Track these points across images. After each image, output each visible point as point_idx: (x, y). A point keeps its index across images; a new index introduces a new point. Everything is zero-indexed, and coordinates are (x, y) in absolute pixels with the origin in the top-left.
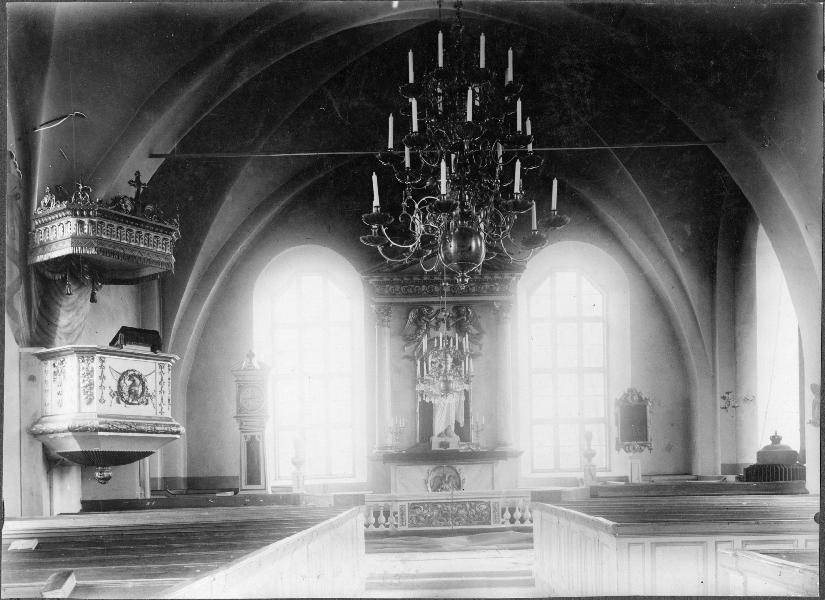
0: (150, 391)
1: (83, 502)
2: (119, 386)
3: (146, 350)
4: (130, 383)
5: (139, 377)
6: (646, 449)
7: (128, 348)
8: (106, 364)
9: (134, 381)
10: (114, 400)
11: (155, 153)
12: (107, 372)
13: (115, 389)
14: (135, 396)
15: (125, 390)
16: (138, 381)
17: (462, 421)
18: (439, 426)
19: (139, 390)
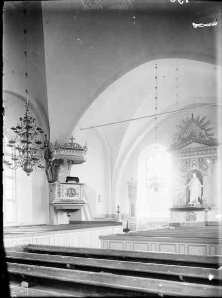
0: (77, 192)
1: (70, 221)
3: (75, 182)
7: (69, 182)
11: (82, 128)
13: (66, 192)
15: (69, 193)
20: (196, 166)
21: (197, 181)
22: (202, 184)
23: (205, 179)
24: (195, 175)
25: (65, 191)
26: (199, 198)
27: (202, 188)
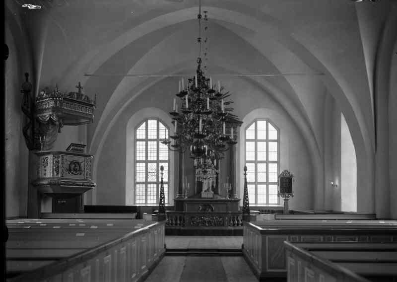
0: (83, 169)
2: (70, 167)
5: (78, 163)
6: (291, 197)
10: (67, 173)
14: (75, 170)
15: (72, 168)
16: (77, 164)
17: (215, 185)
18: (205, 188)
19: (78, 168)
25: (67, 164)
26: (213, 186)
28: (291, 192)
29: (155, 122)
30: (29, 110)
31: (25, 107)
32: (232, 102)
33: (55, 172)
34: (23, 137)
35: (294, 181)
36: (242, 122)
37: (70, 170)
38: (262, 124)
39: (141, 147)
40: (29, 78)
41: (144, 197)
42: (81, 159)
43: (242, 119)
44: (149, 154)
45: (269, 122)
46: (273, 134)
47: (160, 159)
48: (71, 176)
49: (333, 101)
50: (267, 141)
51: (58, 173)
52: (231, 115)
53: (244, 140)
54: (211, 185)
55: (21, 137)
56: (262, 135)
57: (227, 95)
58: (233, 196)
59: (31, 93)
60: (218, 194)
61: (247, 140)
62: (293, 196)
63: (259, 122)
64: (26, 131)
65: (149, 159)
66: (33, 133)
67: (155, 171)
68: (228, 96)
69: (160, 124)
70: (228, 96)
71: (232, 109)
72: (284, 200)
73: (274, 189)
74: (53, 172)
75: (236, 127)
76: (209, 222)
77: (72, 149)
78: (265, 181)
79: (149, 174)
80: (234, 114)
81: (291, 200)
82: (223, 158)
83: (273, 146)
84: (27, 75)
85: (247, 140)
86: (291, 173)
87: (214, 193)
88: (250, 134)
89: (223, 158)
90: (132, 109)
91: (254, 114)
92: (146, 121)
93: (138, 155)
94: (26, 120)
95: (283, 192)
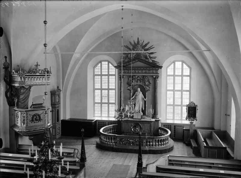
0: (42, 118)
4: (35, 117)
8: (28, 114)
9: (37, 117)
12: (29, 116)
16: (38, 117)
17: (144, 109)
19: (38, 118)
20: (140, 82)
21: (140, 95)
22: (145, 97)
23: (149, 94)
24: (139, 89)
26: (142, 109)
27: (145, 102)
28: (196, 118)
29: (107, 63)
30: (8, 80)
31: (6, 78)
32: (155, 53)
33: (22, 123)
34: (5, 98)
35: (198, 109)
36: (162, 67)
37: (32, 120)
38: (178, 64)
39: (105, 71)
40: (7, 59)
41: (100, 112)
42: (40, 112)
43: (162, 64)
44: (103, 84)
45: (183, 63)
46: (187, 71)
47: (110, 87)
48: (33, 124)
49: (227, 85)
50: (182, 76)
51: (24, 124)
52: (154, 61)
53: (165, 75)
54: (141, 109)
55: (4, 96)
56: (105, 72)
57: (152, 47)
58: (156, 117)
59: (9, 69)
60: (145, 114)
61: (167, 76)
62: (196, 120)
63: (176, 63)
64: (7, 93)
65: (103, 88)
66: (12, 94)
67: (107, 96)
68: (153, 48)
69: (110, 64)
70: (153, 48)
71: (156, 57)
72: (190, 123)
73: (185, 114)
74: (21, 123)
75: (158, 70)
76: (133, 142)
77: (33, 107)
78: (180, 104)
79: (103, 97)
80: (156, 61)
81: (195, 122)
82: (149, 90)
83: (186, 80)
84: (6, 57)
85: (167, 76)
86: (196, 104)
87: (143, 114)
88: (170, 71)
89: (149, 90)
90: (90, 57)
91: (172, 58)
92: (101, 62)
93: (96, 85)
94: (7, 87)
95: (190, 117)
